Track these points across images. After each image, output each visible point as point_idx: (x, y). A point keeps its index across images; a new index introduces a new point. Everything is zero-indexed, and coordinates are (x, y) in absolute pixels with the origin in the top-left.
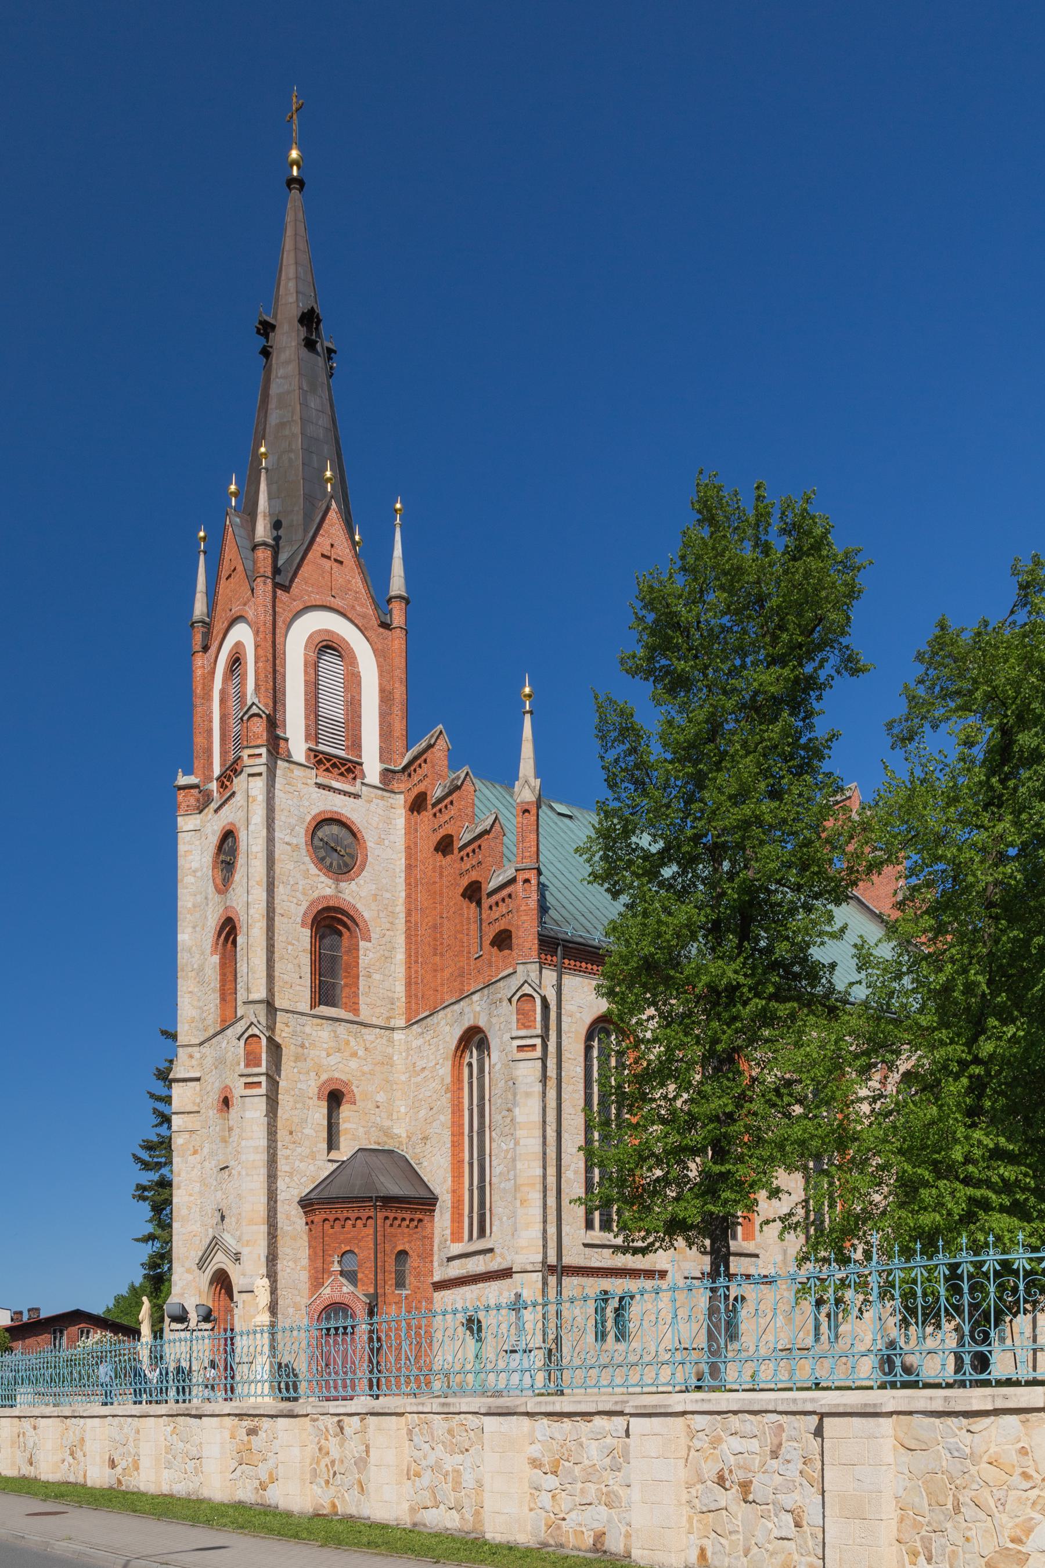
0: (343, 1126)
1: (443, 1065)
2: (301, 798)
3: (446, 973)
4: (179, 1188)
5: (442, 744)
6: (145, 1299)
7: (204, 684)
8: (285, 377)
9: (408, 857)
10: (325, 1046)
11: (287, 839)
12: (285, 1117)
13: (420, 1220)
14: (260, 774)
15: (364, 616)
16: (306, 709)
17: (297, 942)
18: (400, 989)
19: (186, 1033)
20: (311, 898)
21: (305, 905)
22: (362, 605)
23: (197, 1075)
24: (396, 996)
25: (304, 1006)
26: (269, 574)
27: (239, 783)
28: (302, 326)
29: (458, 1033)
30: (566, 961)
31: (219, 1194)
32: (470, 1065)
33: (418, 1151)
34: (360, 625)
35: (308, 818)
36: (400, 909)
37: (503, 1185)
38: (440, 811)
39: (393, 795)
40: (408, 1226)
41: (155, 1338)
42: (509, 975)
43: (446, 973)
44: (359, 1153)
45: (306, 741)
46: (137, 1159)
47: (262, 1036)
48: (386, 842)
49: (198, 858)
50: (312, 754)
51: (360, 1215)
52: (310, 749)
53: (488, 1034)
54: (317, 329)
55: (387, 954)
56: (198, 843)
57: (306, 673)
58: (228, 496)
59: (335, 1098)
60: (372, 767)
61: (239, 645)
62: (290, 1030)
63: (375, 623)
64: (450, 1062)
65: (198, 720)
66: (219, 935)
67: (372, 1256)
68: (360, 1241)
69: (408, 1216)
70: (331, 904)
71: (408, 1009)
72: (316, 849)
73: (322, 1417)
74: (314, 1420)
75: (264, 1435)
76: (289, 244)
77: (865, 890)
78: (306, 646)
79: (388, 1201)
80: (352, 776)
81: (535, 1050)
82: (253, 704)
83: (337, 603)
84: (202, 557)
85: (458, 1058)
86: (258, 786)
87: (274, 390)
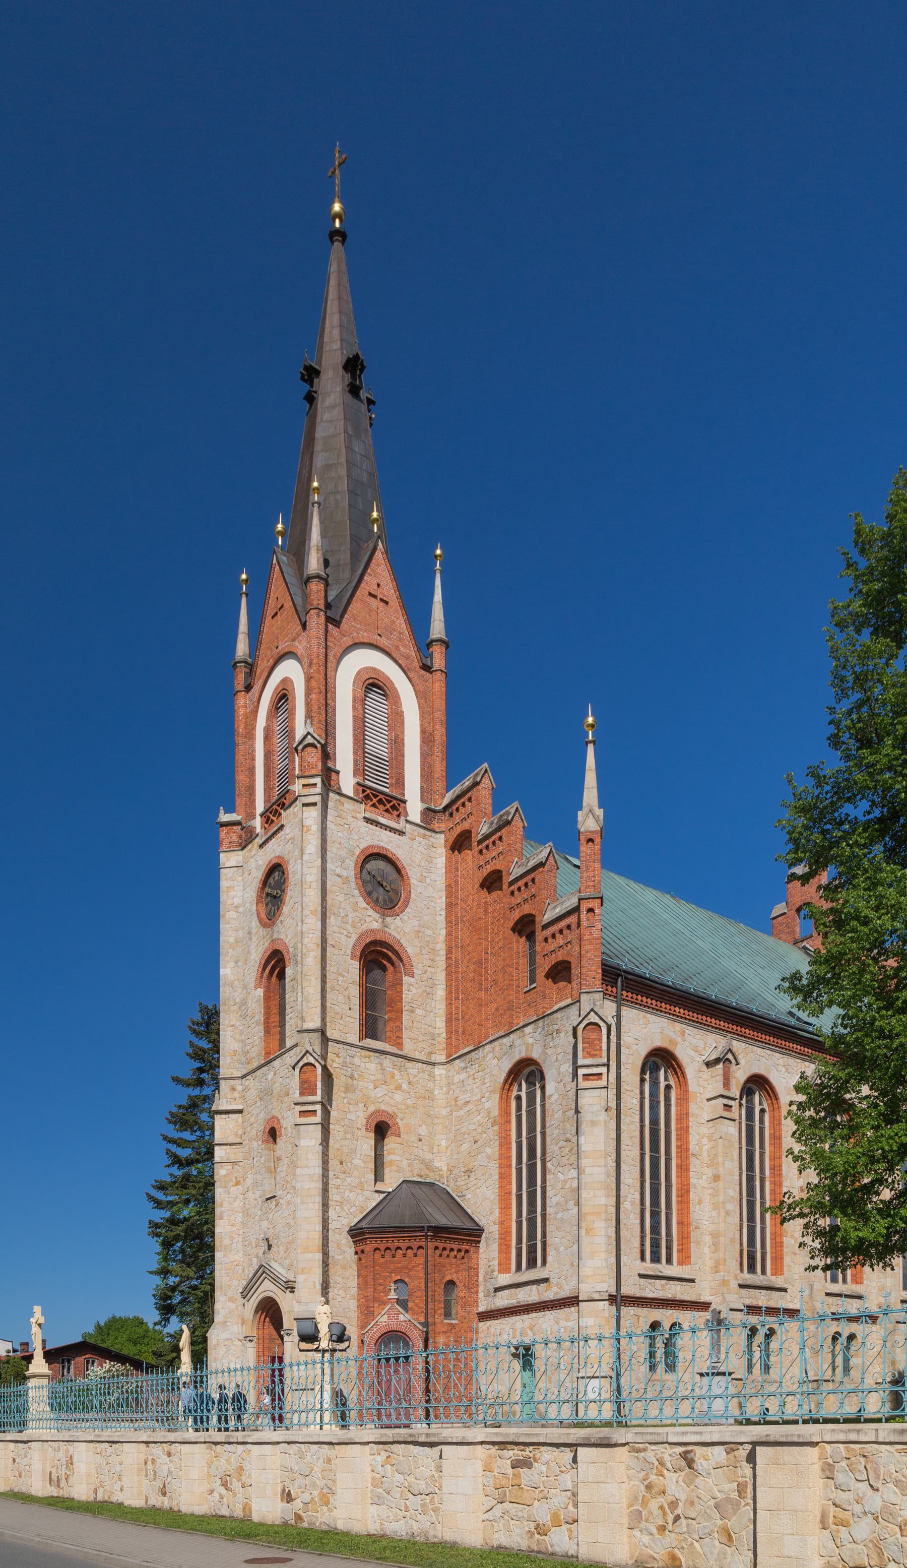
0: (387, 1158)
1: (489, 1098)
2: (350, 831)
3: (492, 1008)
4: (221, 1218)
5: (486, 783)
8: (331, 421)
9: (448, 896)
10: (373, 1078)
11: (338, 871)
12: (336, 1146)
13: (467, 1251)
14: (314, 804)
15: (407, 657)
16: (354, 744)
17: (347, 972)
18: (441, 1025)
19: (228, 1065)
20: (359, 931)
21: (354, 937)
22: (405, 646)
23: (240, 1107)
24: (437, 1031)
25: (353, 1038)
26: (322, 607)
27: (288, 816)
28: (347, 373)
29: (507, 1065)
30: (624, 993)
31: (265, 1224)
32: (519, 1098)
33: (460, 1183)
34: (404, 665)
35: (358, 852)
36: (441, 947)
37: (560, 1215)
38: (487, 847)
39: (434, 834)
40: (455, 1257)
41: (195, 1369)
42: (568, 1006)
43: (492, 1008)
44: (404, 1185)
45: (355, 775)
46: (151, 1198)
47: (317, 1064)
48: (428, 880)
49: (240, 894)
50: (361, 789)
51: (411, 1244)
52: (359, 784)
53: (543, 1066)
54: (360, 376)
56: (240, 879)
57: (354, 708)
58: (274, 535)
59: (381, 1130)
60: (414, 808)
61: (286, 681)
62: (340, 1060)
63: (416, 664)
64: (498, 1096)
65: (240, 758)
67: (423, 1286)
68: (410, 1270)
69: (455, 1246)
70: (378, 938)
71: (449, 1044)
72: (364, 882)
73: (653, 1447)
74: (638, 1451)
75: (544, 1468)
76: (332, 293)
78: (354, 682)
79: (439, 1231)
80: (396, 813)
83: (383, 642)
84: (244, 600)
86: (312, 816)
87: (320, 433)
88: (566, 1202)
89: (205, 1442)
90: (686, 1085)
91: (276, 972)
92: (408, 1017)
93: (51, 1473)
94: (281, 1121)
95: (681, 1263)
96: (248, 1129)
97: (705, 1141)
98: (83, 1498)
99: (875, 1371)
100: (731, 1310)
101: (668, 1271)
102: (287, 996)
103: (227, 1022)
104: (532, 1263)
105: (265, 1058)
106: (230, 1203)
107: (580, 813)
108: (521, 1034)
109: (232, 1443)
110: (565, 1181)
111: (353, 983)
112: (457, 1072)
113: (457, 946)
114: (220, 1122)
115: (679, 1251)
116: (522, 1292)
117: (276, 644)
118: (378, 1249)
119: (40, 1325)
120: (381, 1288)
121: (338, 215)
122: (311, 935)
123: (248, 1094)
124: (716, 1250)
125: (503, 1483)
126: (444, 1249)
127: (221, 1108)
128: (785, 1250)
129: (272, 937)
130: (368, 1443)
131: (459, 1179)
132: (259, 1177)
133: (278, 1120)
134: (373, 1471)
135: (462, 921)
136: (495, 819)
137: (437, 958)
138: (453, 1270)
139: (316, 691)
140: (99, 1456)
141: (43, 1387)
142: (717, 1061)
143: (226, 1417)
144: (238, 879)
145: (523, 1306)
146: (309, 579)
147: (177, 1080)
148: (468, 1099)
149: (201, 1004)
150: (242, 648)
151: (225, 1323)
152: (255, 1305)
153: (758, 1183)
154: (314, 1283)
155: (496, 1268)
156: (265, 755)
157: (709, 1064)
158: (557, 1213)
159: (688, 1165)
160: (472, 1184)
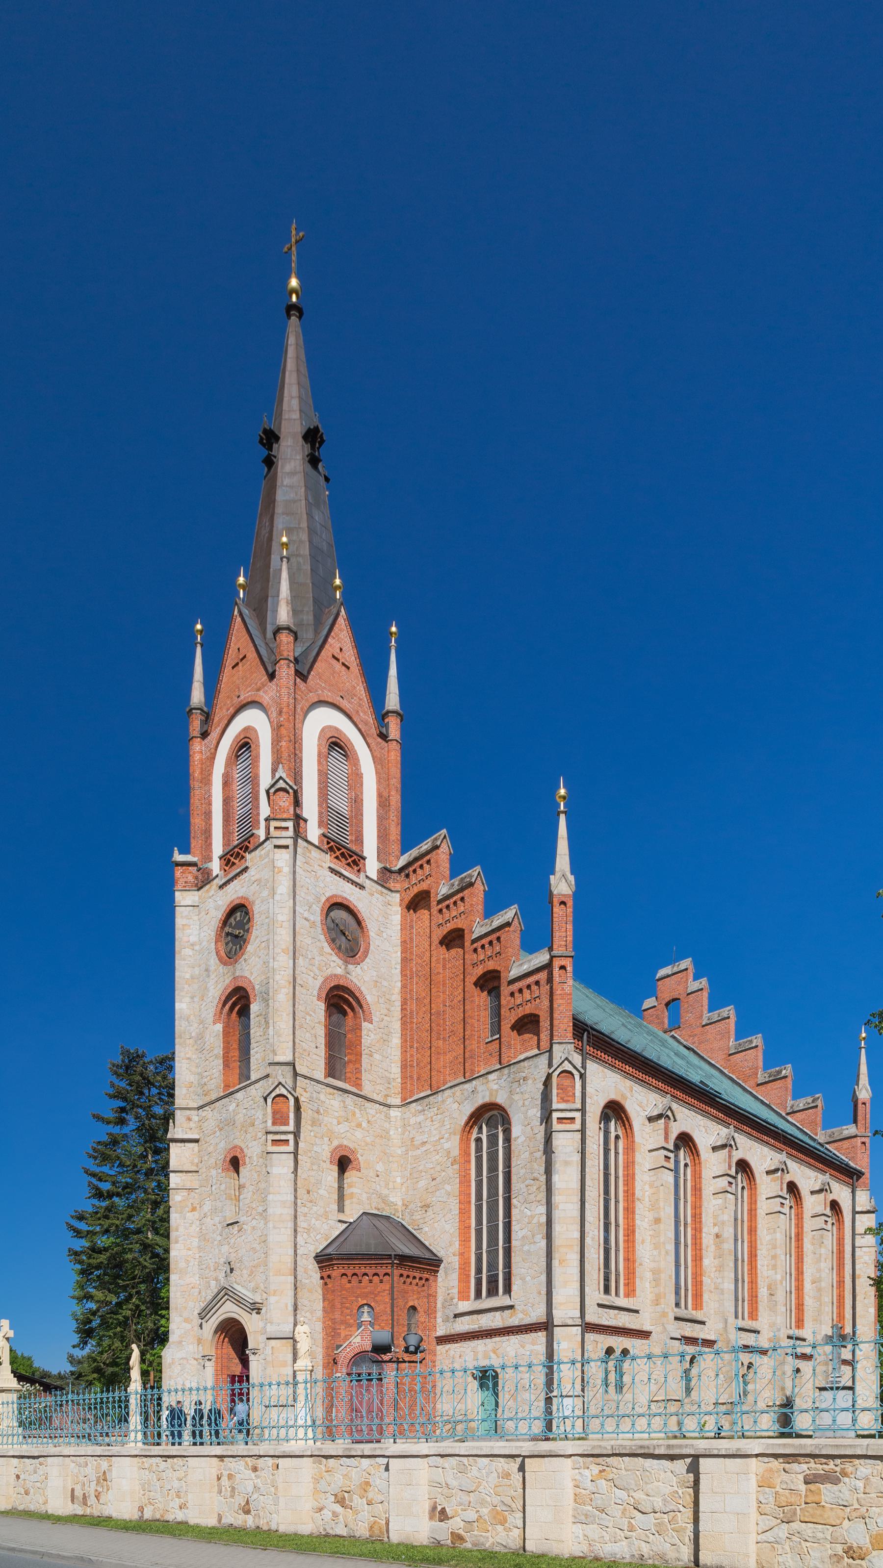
1: (448, 1139)
4: (177, 1242)
5: (445, 849)
6: (134, 1346)
7: (202, 768)
8: (291, 487)
10: (336, 1114)
11: (306, 915)
13: (427, 1280)
14: (287, 847)
15: (366, 723)
18: (396, 1070)
20: (325, 974)
21: (320, 980)
22: (365, 713)
23: (196, 1137)
24: (392, 1076)
25: (320, 1074)
28: (306, 443)
29: (469, 1109)
31: (225, 1249)
32: (479, 1140)
34: (363, 730)
35: (323, 899)
36: (397, 998)
37: (526, 1248)
39: (389, 893)
40: (417, 1285)
47: (289, 1096)
48: (384, 934)
50: (325, 840)
51: (367, 1271)
53: (508, 1110)
55: (385, 1037)
56: (196, 918)
60: (372, 866)
62: (308, 1095)
63: (374, 732)
64: (458, 1137)
65: (195, 801)
66: (224, 1005)
68: (376, 1295)
69: (418, 1275)
70: (341, 983)
75: (860, 1484)
77: (700, 1044)
78: (319, 738)
79: (404, 1260)
80: (356, 868)
81: (574, 1123)
82: (281, 778)
83: (344, 704)
85: (466, 1133)
88: (533, 1236)
89: (311, 1456)
90: (633, 1137)
93: (73, 1490)
94: (245, 1150)
95: (627, 1295)
97: (647, 1187)
98: (127, 1516)
99: (766, 1395)
100: (672, 1338)
101: (622, 1302)
102: (252, 1032)
103: (182, 1055)
104: (478, 1295)
105: (224, 1091)
107: (552, 877)
108: (485, 1081)
109: (353, 1456)
110: (532, 1217)
111: (319, 1023)
113: (412, 998)
114: (175, 1150)
115: (625, 1285)
116: (485, 1318)
117: (237, 694)
118: (366, 1274)
119: (8, 1339)
120: (348, 1311)
121: (293, 291)
122: (283, 973)
123: (206, 1124)
124: (657, 1285)
125: (793, 1500)
126: (408, 1276)
127: (176, 1136)
128: (704, 1288)
130: (571, 1456)
131: (416, 1214)
132: (219, 1204)
133: (241, 1149)
134: (577, 1486)
136: (456, 881)
137: (392, 1009)
138: (415, 1297)
139: (286, 739)
140: (147, 1472)
141: (205, 1389)
142: (660, 1116)
143: (201, 1432)
144: (195, 919)
145: (486, 1331)
146: (278, 630)
147: (97, 1117)
148: (425, 1140)
150: (197, 696)
151: (180, 1342)
152: (215, 1326)
153: (682, 1228)
155: (456, 1296)
156: (224, 800)
157: (651, 1119)
158: (523, 1246)
159: (634, 1208)
160: (430, 1218)
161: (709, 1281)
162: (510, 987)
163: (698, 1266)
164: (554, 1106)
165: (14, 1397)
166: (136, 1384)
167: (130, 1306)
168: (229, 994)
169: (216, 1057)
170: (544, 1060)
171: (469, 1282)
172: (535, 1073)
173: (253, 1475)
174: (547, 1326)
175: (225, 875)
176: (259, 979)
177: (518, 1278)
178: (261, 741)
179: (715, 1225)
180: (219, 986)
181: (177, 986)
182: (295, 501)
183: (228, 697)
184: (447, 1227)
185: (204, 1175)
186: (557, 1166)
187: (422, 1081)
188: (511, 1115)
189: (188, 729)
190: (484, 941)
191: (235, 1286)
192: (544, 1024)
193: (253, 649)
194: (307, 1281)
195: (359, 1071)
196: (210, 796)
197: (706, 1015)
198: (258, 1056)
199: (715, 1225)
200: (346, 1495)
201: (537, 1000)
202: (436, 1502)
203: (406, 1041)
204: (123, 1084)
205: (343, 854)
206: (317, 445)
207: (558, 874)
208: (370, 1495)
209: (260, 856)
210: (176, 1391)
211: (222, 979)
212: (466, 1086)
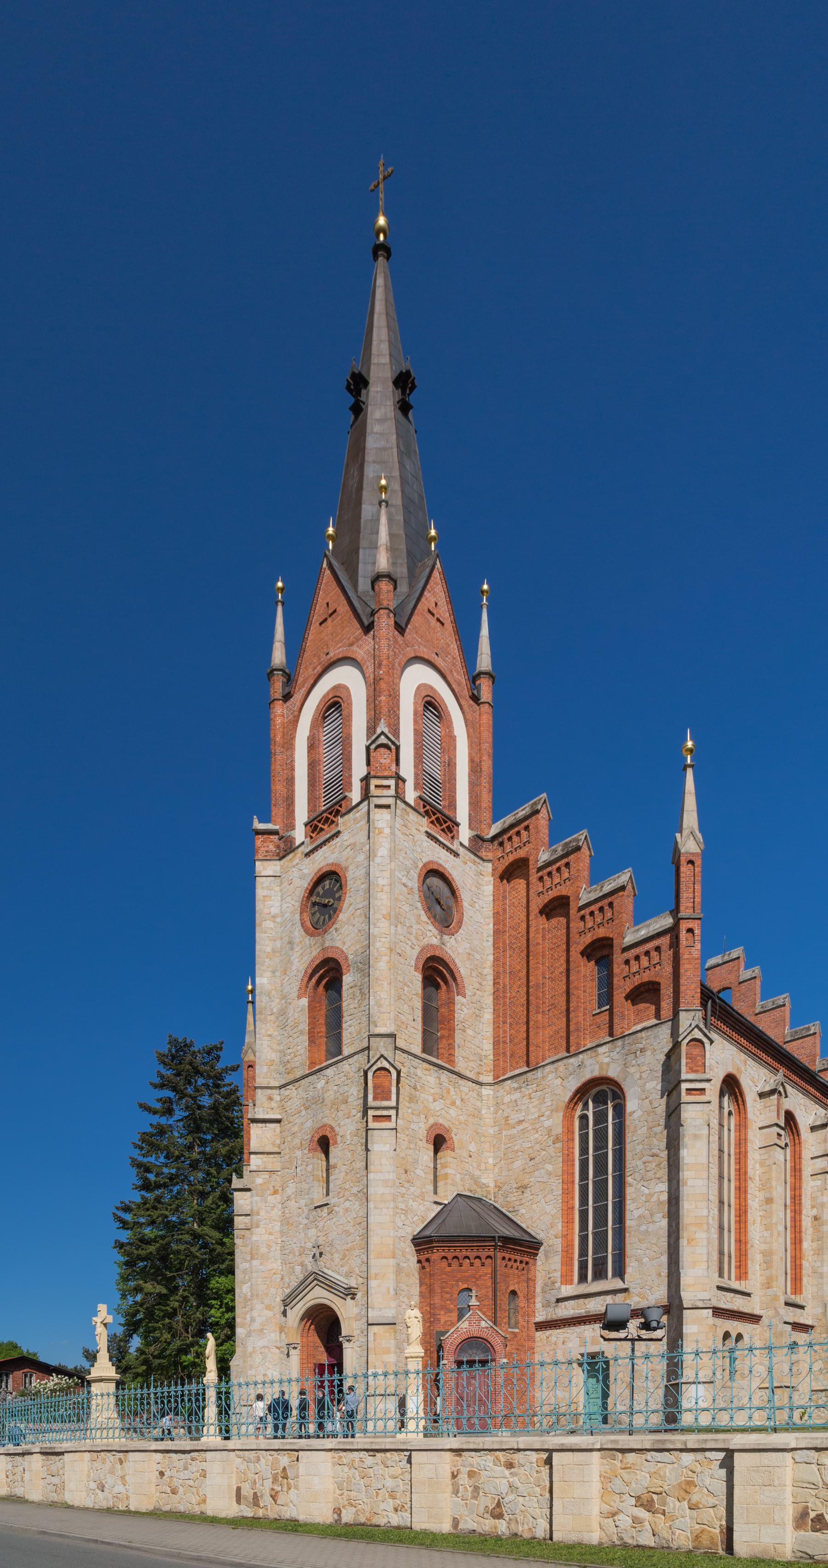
1: (549, 1117)
6: (209, 1335)
7: (283, 733)
10: (432, 1091)
11: (404, 880)
13: (527, 1263)
15: (459, 684)
18: (488, 1047)
20: (422, 944)
21: (418, 949)
22: (458, 673)
23: (278, 1117)
24: (484, 1053)
25: (417, 1049)
29: (574, 1084)
31: (312, 1232)
32: (584, 1118)
34: (456, 691)
35: (420, 865)
37: (643, 1228)
39: (481, 862)
48: (477, 905)
49: (278, 904)
50: (422, 803)
51: (468, 1254)
55: (477, 1012)
56: (278, 889)
58: (325, 538)
60: (465, 834)
63: (466, 693)
64: (562, 1114)
65: (277, 766)
66: (310, 979)
67: (490, 1294)
68: (477, 1279)
69: (518, 1258)
70: (437, 953)
78: (415, 696)
79: (507, 1241)
82: (383, 733)
83: (439, 662)
84: (280, 609)
88: (652, 1215)
90: (745, 1113)
91: (324, 982)
92: (461, 1036)
93: (239, 1489)
94: (337, 1129)
95: (739, 1278)
96: (289, 1139)
97: (758, 1166)
101: (735, 1285)
102: (344, 1004)
104: (583, 1278)
105: (310, 1068)
106: (267, 1212)
108: (594, 1054)
110: (651, 1195)
111: (416, 994)
112: (508, 1093)
113: (505, 972)
115: (736, 1267)
116: (594, 1302)
117: (326, 651)
119: (105, 1325)
120: (448, 1296)
121: (381, 230)
122: (383, 940)
123: (289, 1103)
127: (260, 1116)
128: (804, 1272)
129: (322, 945)
132: (305, 1186)
133: (332, 1128)
135: (511, 947)
137: (484, 983)
140: (346, 1469)
142: (773, 1092)
144: (278, 891)
149: (170, 1036)
150: (278, 656)
151: (262, 1330)
152: (301, 1313)
154: (389, 1288)
155: (559, 1280)
159: (746, 1187)
160: (528, 1199)
161: (807, 1265)
162: (625, 954)
163: (798, 1249)
164: (684, 1076)
165: (112, 1387)
166: (211, 1375)
167: (177, 1298)
168: (317, 966)
169: (302, 1032)
170: (665, 1031)
171: (572, 1265)
172: (655, 1044)
173: (507, 1472)
174: (674, 1308)
175: (312, 843)
176: (353, 948)
177: (633, 1259)
178: (353, 699)
179: (813, 1207)
180: (305, 958)
181: (258, 960)
182: (384, 449)
183: (315, 655)
184: (548, 1208)
185: (287, 1157)
186: (686, 1139)
187: (519, 1056)
188: (625, 1089)
189: (269, 691)
190: (592, 908)
191: (325, 1270)
192: (667, 992)
193: (345, 602)
194: (405, 1265)
195: (451, 1047)
196: (293, 761)
197: (759, 1004)
198: (352, 1029)
199: (813, 1207)
200: (655, 1497)
201: (658, 967)
202: (807, 1507)
203: (498, 1016)
204: (168, 1073)
205: (437, 819)
206: (408, 392)
207: (685, 832)
208: (695, 1498)
209: (355, 819)
210: (256, 1384)
211: (308, 951)
212: (572, 1060)
